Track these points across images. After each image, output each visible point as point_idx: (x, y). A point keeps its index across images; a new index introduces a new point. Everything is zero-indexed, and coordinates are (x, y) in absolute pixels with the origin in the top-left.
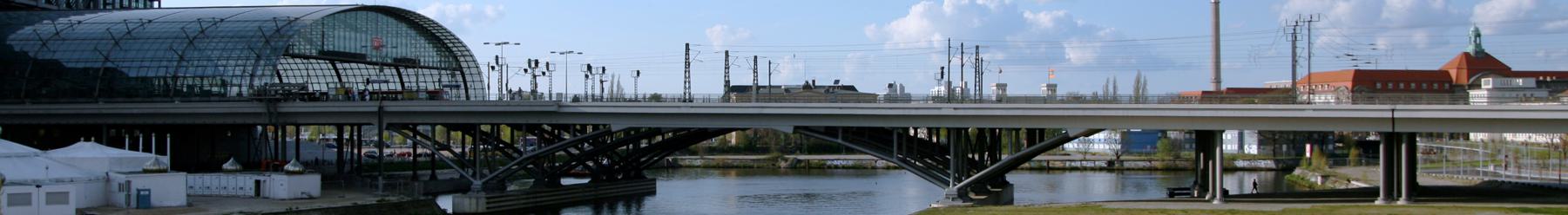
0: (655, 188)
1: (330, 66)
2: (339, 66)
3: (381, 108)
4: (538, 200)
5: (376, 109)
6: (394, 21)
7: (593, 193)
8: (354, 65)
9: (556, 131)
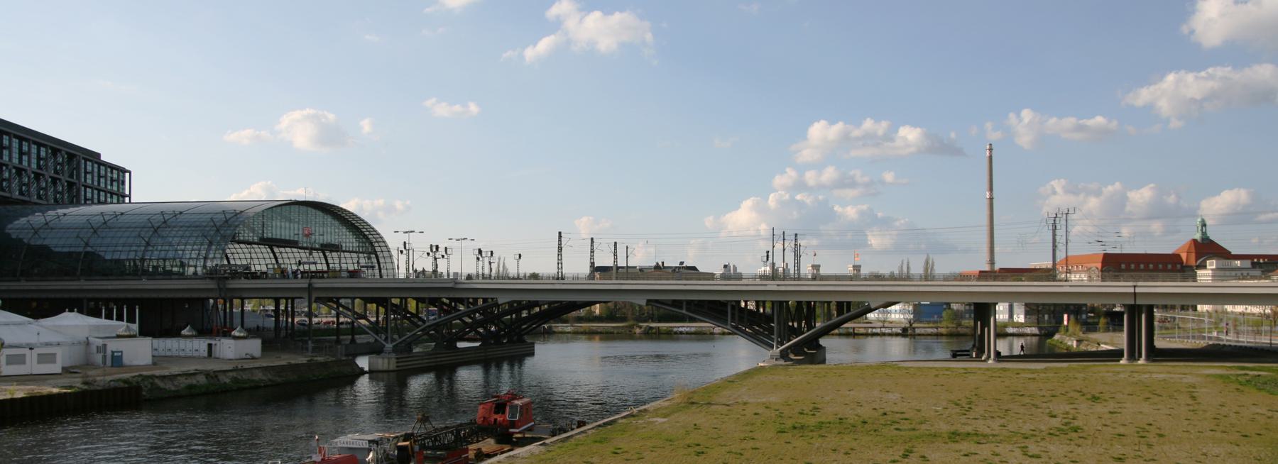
0: (534, 350)
1: (269, 250)
2: (276, 250)
3: (310, 284)
4: (439, 360)
5: (306, 286)
6: (321, 214)
7: (482, 354)
8: (288, 250)
9: (453, 304)
